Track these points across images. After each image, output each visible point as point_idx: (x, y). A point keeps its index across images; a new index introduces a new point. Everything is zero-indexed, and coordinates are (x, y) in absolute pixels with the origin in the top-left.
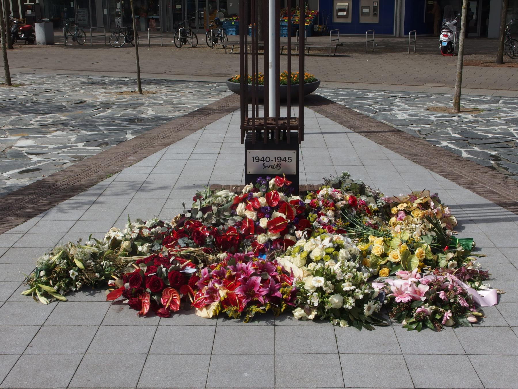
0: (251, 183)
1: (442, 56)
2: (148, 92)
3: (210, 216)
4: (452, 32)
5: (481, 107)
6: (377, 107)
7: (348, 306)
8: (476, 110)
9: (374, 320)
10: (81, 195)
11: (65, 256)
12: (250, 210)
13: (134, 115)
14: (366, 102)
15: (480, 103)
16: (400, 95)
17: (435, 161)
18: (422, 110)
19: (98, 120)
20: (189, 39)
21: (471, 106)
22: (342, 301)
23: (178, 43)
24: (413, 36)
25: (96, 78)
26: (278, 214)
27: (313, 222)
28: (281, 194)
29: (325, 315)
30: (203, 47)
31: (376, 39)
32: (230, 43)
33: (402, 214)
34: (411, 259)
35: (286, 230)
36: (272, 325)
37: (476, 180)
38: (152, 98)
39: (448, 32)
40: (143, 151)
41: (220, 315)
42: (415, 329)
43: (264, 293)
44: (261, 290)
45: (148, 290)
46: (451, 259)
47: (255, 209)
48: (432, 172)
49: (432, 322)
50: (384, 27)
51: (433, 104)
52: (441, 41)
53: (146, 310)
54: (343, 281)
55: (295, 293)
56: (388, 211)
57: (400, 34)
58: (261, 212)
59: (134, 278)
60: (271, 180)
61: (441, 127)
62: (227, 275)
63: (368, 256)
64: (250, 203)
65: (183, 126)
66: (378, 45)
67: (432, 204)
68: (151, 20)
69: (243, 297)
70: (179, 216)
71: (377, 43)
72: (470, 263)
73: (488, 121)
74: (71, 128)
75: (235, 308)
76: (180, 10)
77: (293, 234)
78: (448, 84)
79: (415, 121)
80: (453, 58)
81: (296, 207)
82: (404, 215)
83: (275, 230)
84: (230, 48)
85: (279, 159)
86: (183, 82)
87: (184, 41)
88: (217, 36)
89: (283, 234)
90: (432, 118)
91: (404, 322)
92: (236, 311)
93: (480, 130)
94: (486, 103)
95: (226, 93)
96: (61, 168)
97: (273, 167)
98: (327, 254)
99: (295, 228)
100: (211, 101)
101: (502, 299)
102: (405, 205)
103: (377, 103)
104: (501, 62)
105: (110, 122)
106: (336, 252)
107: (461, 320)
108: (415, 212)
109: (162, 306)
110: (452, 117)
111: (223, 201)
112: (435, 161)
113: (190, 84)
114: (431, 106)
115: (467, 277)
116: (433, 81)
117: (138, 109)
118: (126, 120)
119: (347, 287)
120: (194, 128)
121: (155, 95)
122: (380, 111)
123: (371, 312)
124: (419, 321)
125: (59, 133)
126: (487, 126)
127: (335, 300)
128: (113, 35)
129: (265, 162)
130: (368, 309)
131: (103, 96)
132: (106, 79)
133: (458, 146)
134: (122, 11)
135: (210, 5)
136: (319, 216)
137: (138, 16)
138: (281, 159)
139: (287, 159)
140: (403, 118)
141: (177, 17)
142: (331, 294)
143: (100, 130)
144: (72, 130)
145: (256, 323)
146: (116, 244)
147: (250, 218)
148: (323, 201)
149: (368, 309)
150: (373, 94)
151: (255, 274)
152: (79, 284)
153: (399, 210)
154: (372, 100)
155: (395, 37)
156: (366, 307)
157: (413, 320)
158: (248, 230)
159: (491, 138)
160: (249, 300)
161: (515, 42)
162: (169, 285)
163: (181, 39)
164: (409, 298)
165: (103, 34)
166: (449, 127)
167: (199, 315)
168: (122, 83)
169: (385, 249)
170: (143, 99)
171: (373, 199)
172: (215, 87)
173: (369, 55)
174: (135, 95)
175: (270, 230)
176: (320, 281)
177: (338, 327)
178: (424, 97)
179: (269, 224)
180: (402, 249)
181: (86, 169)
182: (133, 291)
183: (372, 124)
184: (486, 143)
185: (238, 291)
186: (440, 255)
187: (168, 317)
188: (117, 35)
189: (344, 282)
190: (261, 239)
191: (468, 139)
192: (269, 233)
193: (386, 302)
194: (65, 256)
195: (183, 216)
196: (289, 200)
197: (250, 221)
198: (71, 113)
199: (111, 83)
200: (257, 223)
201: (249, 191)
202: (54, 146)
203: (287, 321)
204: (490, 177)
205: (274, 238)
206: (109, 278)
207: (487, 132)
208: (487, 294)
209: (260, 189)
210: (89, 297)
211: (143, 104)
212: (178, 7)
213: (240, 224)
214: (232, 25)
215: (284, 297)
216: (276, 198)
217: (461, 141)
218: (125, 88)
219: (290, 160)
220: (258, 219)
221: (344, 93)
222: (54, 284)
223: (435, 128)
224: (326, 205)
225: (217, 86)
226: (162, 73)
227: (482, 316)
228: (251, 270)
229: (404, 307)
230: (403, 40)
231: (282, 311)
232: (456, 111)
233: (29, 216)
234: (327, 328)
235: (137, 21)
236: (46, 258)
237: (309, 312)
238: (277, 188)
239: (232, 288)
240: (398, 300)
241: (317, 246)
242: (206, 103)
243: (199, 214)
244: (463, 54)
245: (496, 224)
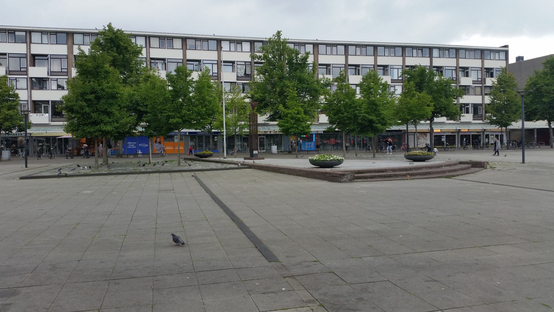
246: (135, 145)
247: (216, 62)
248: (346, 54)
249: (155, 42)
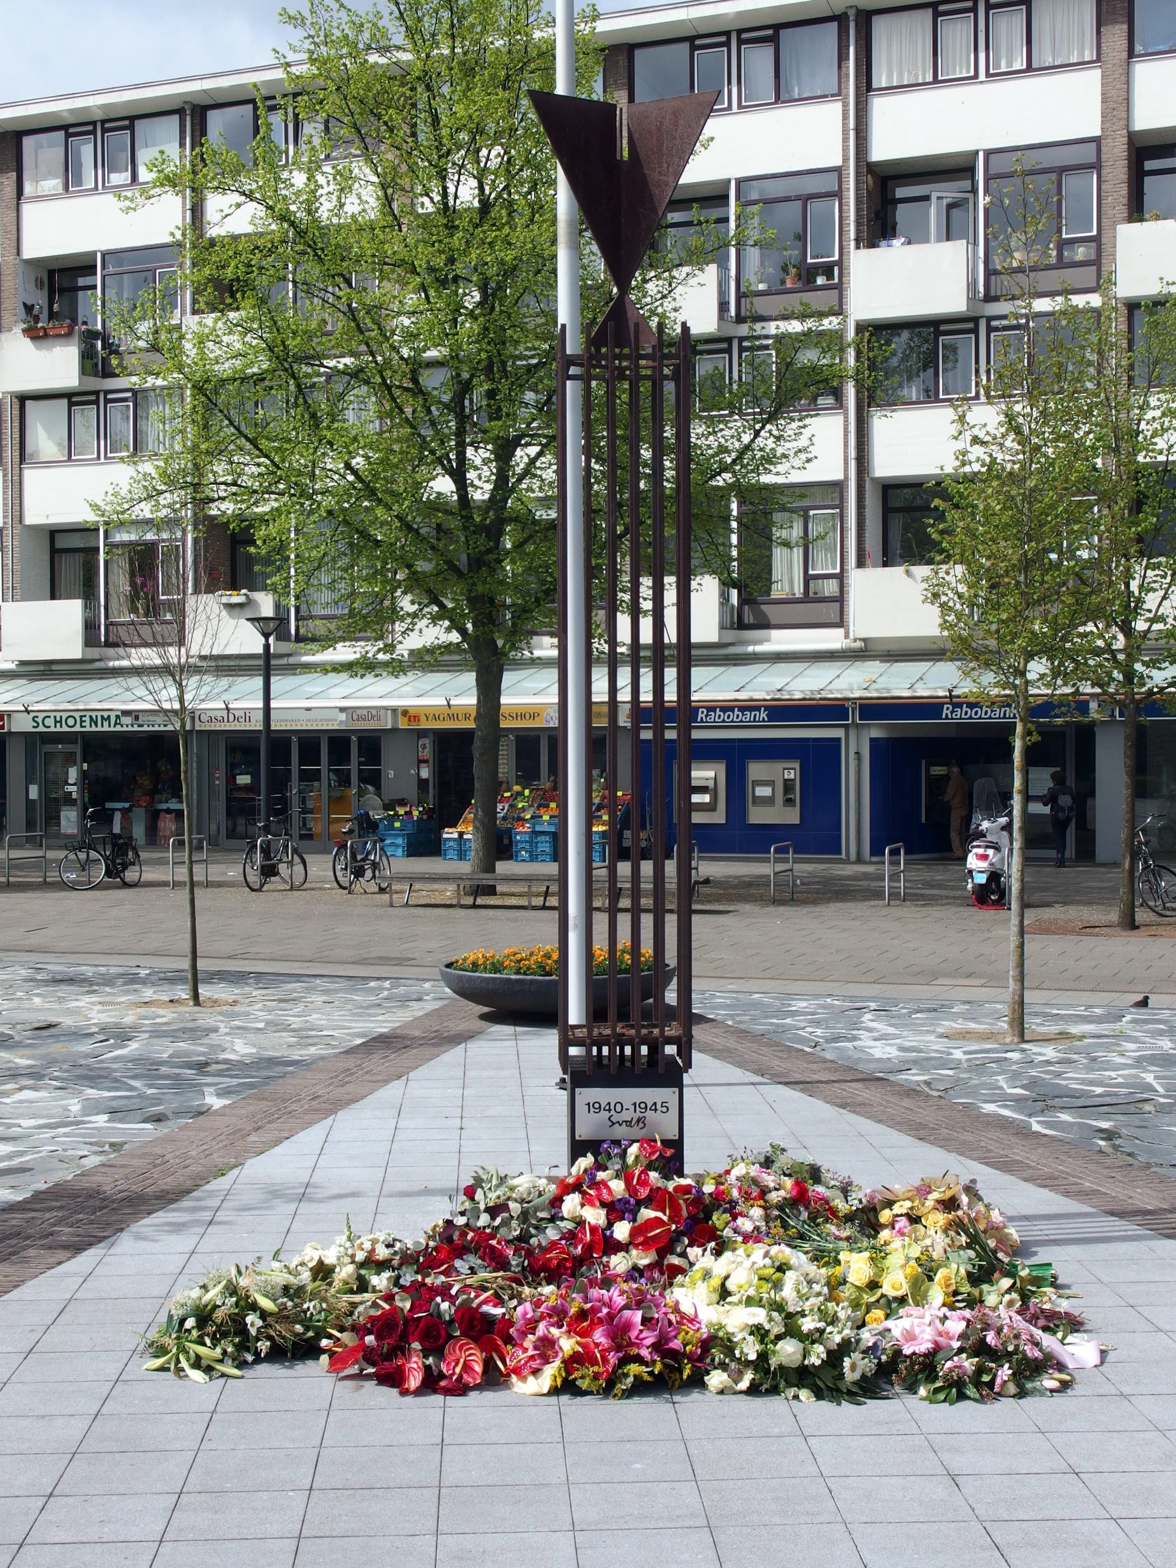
0: (589, 1155)
1: (976, 909)
2: (215, 1003)
3: (506, 1223)
4: (997, 848)
5: (1075, 1030)
6: (819, 1032)
7: (814, 1360)
8: (1064, 1036)
9: (861, 1388)
10: (174, 1210)
11: (232, 1289)
12: (592, 1205)
13: (203, 1054)
14: (788, 1021)
15: (1076, 1023)
16: (873, 1005)
17: (969, 1137)
18: (932, 1038)
19: (115, 1066)
20: (283, 868)
21: (1053, 1029)
22: (801, 1351)
23: (254, 877)
24: (894, 858)
25: (57, 967)
26: (647, 1213)
27: (722, 1231)
28: (653, 1175)
29: (769, 1380)
30: (321, 889)
31: (797, 867)
32: (401, 879)
33: (903, 1223)
34: (927, 1291)
35: (666, 1247)
36: (667, 1401)
37: (1062, 1172)
38: (233, 1016)
39: (987, 847)
40: (275, 1125)
41: (566, 1387)
42: (945, 1401)
43: (648, 1342)
44: (642, 1336)
45: (416, 1345)
46: (1008, 1291)
47: (603, 1205)
48: (962, 1158)
49: (976, 1387)
50: (817, 833)
51: (959, 1025)
52: (970, 872)
53: (414, 1382)
54: (803, 1314)
55: (707, 1344)
56: (873, 1220)
57: (859, 853)
58: (616, 1210)
59: (385, 1325)
60: (630, 1145)
61: (981, 1075)
62: (573, 1311)
63: (841, 1288)
64: (591, 1192)
65: (352, 1074)
66: (802, 884)
67: (965, 1199)
68: (162, 814)
69: (609, 1350)
70: (441, 1223)
71: (798, 877)
72: (1045, 1299)
73: (1094, 1059)
74: (54, 1083)
75: (596, 1369)
76: (246, 788)
77: (683, 1255)
78: (994, 980)
79: (915, 1062)
80: (1003, 913)
81: (686, 1200)
82: (907, 1224)
83: (646, 1245)
84: (402, 892)
85: (643, 1106)
86: (298, 977)
87: (269, 871)
88: (363, 860)
89: (662, 1253)
90: (958, 1054)
91: (922, 1391)
92: (596, 1376)
93: (1073, 1079)
94: (1090, 1022)
95: (420, 1003)
96: (79, 1166)
97: (629, 1123)
98: (760, 1279)
99: (686, 1241)
100: (389, 1022)
101: (1111, 1357)
102: (908, 1204)
103: (817, 1023)
104: (1130, 923)
105: (148, 1068)
106: (778, 1274)
107: (1029, 1385)
108: (931, 1216)
109: (442, 1376)
110: (1007, 1051)
111: (530, 1193)
112: (969, 1137)
113: (318, 981)
114: (952, 1028)
115: (1042, 1322)
116: (955, 973)
117: (206, 1041)
118: (189, 1065)
119: (808, 1324)
120: (379, 1078)
121: (236, 1009)
122: (827, 1041)
123: (856, 1376)
124: (950, 1386)
125: (27, 1094)
126: (1089, 1069)
127: (788, 1351)
128: (72, 856)
129: (613, 1112)
130: (854, 1368)
131: (99, 1012)
132: (89, 971)
133: (1021, 1112)
134: (82, 791)
135: (332, 776)
136: (734, 1218)
137: (127, 805)
138: (646, 1107)
139: (659, 1106)
140: (885, 1056)
141: (240, 808)
142: (779, 1337)
143: (132, 1088)
144: (60, 1088)
145: (636, 1399)
146: (323, 1272)
147: (593, 1222)
148: (740, 1189)
149: (854, 1368)
150: (804, 1004)
151: (626, 1307)
152: (264, 1346)
153: (897, 1216)
154: (805, 1015)
155: (847, 861)
156: (847, 1362)
157: (939, 1384)
158: (589, 1249)
159: (1100, 1096)
160: (620, 1355)
161: (1167, 877)
162: (458, 1333)
163: (263, 867)
164: (930, 1345)
165: (40, 853)
166: (999, 1074)
167: (520, 1391)
168: (132, 979)
169: (875, 1274)
170: (206, 1018)
171: (839, 1193)
172: (388, 989)
173: (782, 908)
174: (182, 1009)
175: (636, 1246)
176: (759, 1316)
177: (795, 1402)
178: (935, 1010)
179: (634, 1233)
180: (908, 1271)
181: (158, 1161)
182: (385, 1350)
183: (814, 1067)
184: (1087, 1106)
185: (599, 1336)
186: (985, 1287)
187: (460, 1395)
188: (82, 856)
189: (804, 1316)
190: (619, 1263)
191: (1043, 1098)
192: (634, 1252)
193: (884, 1358)
194: (232, 1289)
195: (449, 1223)
196: (671, 1186)
197: (594, 1229)
198: (37, 1052)
199: (109, 981)
200: (608, 1233)
201: (586, 1171)
202: (33, 1122)
203: (696, 1395)
204: (1092, 1167)
205: (645, 1261)
206: (321, 1333)
207: (1091, 1083)
208: (1080, 1351)
209: (609, 1164)
210: (285, 1370)
211: (216, 1030)
212: (244, 780)
213: (571, 1236)
214: (393, 829)
215: (688, 1348)
216: (643, 1183)
217: (1029, 1103)
218: (148, 993)
219: (665, 1109)
220: (610, 1225)
221: (728, 1001)
222: (215, 1346)
223: (965, 1076)
224: (747, 1196)
225: (392, 987)
226: (229, 957)
227: (1071, 1381)
228: (620, 1301)
229: (920, 1364)
230: (870, 869)
231: (685, 1377)
232: (1016, 1040)
233: (77, 1248)
234: (775, 1404)
235: (123, 816)
236: (196, 1293)
237: (737, 1377)
238: (645, 1163)
239: (584, 1333)
240: (907, 1351)
241: (742, 1266)
242: (382, 1023)
243: (484, 1219)
244: (1025, 905)
245: (1104, 1246)
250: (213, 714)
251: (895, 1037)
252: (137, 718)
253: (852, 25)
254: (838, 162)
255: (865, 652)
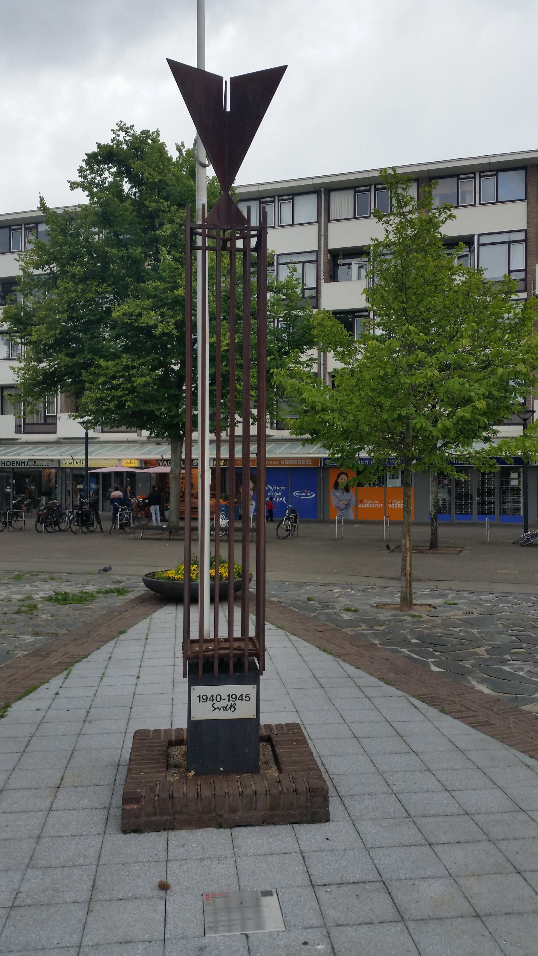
85: (234, 696)
97: (225, 709)
129: (215, 701)
219: (248, 699)
246: (284, 493)
247: (521, 236)
248: (324, 217)
249: (342, 204)
250: (68, 461)
251: (363, 630)
252: (35, 462)
253: (323, 195)
254: (316, 248)
255: (60, 442)
